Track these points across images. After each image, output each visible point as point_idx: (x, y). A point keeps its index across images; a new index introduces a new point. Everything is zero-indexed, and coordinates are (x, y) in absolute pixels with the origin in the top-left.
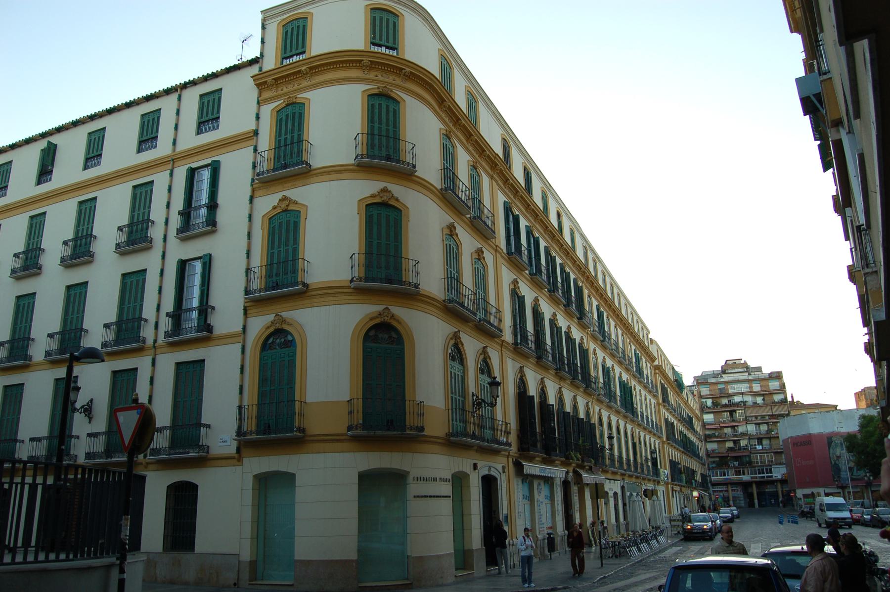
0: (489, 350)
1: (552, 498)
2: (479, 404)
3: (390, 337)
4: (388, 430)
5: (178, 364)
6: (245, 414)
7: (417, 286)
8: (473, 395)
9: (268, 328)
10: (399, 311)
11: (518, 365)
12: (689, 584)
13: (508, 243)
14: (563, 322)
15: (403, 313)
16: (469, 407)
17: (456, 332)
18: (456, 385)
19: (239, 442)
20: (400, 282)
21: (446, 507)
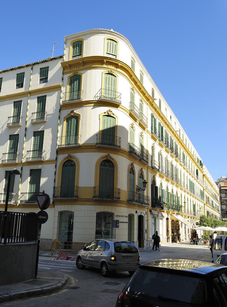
0: (143, 169)
1: (207, 248)
2: (139, 190)
3: (109, 165)
4: (108, 198)
5: (31, 170)
6: (56, 190)
7: (120, 147)
8: (137, 186)
9: (66, 159)
10: (113, 156)
11: (153, 175)
12: (225, 278)
13: (152, 129)
14: (170, 159)
15: (114, 156)
16: (135, 191)
17: (132, 163)
18: (131, 181)
19: (54, 200)
20: (114, 145)
21: (126, 225)
